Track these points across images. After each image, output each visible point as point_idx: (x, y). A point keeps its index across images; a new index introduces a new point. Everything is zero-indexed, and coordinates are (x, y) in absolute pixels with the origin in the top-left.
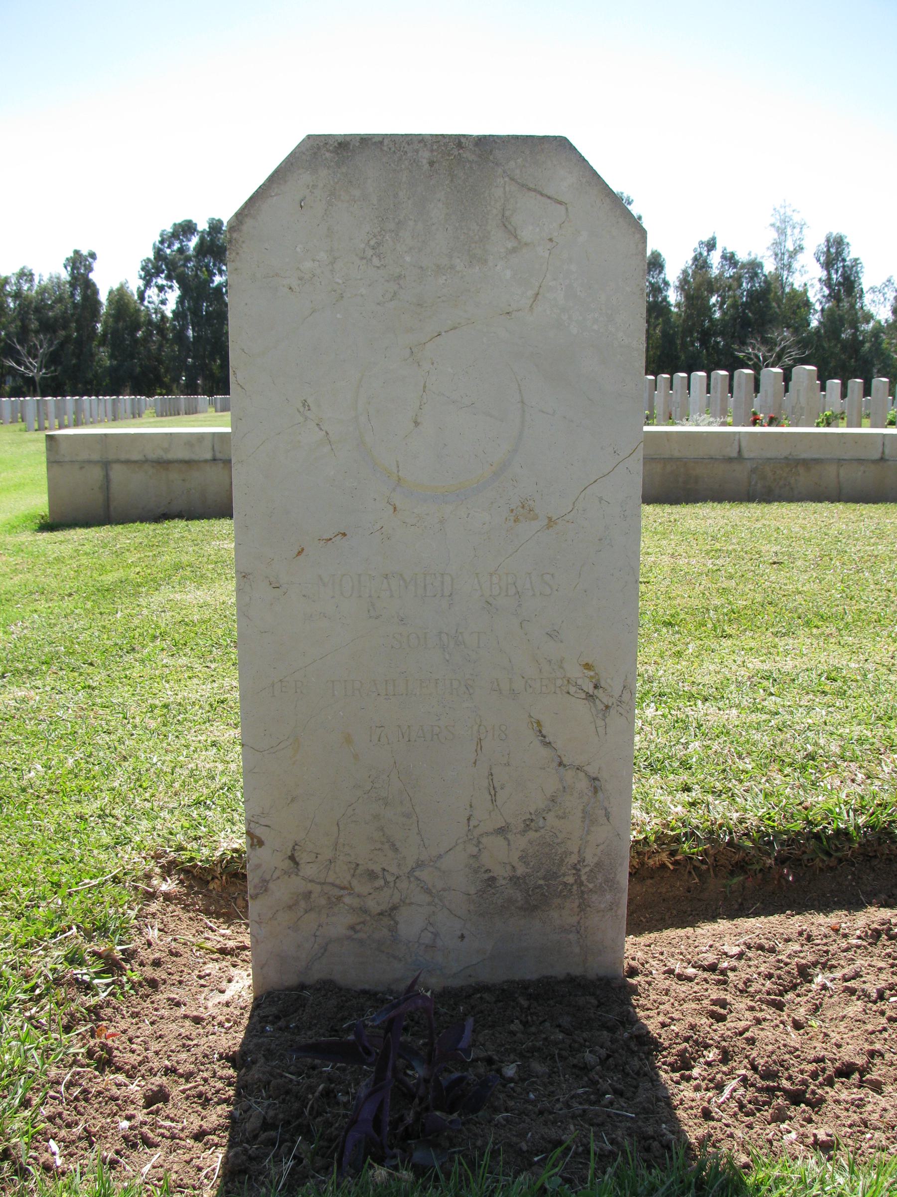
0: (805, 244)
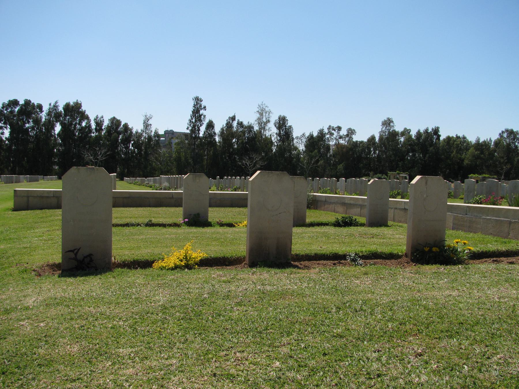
0: (270, 120)
